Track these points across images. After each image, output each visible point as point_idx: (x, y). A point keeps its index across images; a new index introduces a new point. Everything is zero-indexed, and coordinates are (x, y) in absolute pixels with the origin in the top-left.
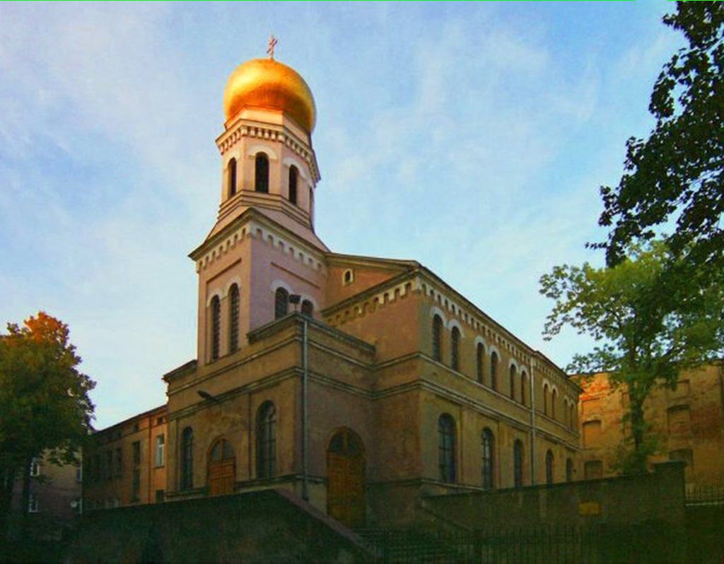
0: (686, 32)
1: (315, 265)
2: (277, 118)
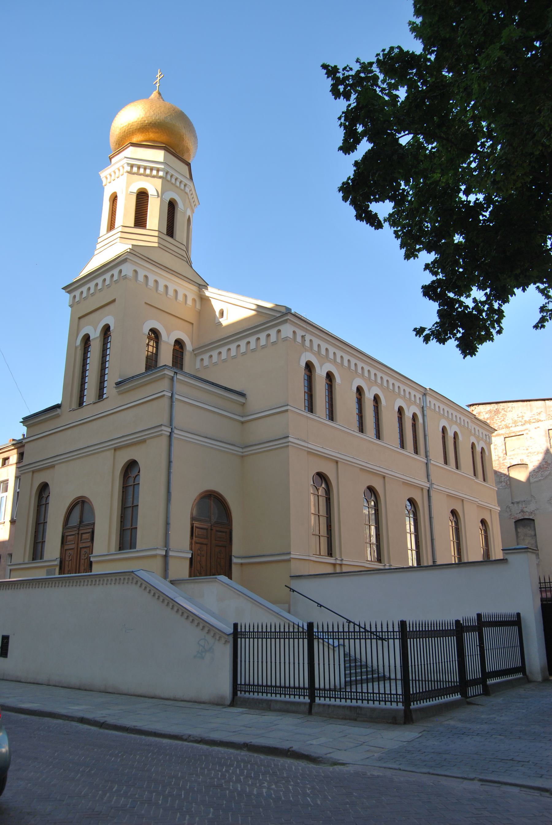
2: (159, 155)
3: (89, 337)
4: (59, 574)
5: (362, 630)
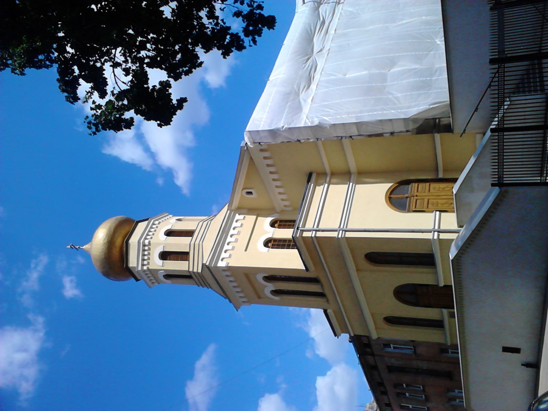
1: (242, 217)
3: (273, 291)
4: (454, 308)
5: (497, 75)
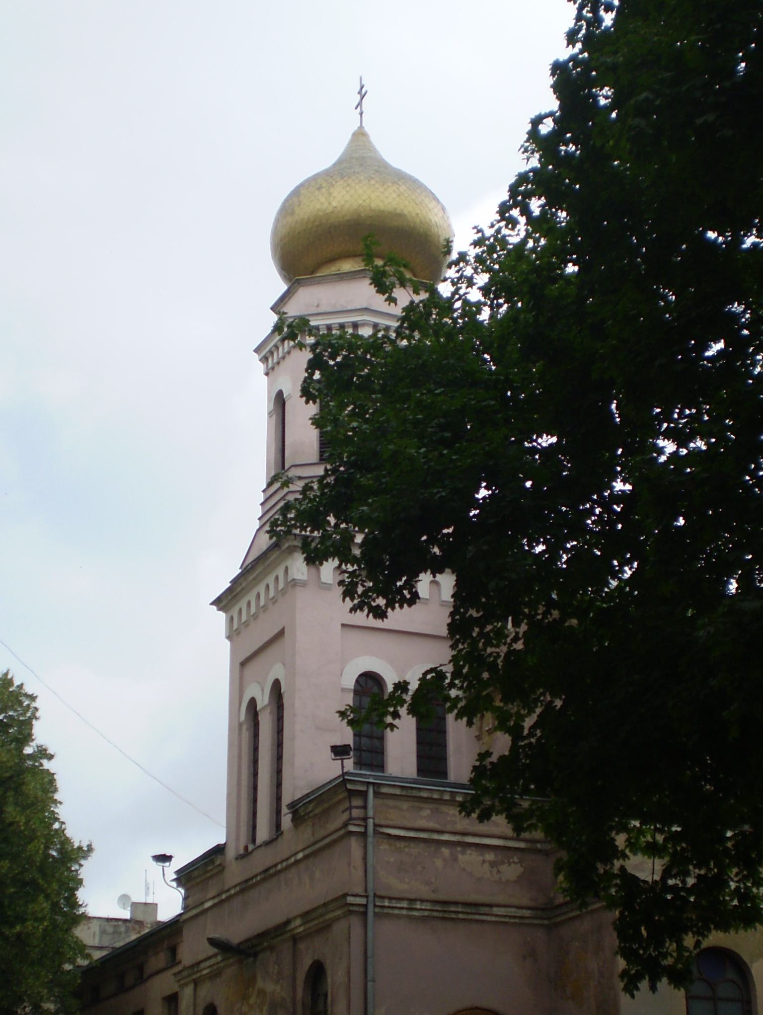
0: (478, 763)
